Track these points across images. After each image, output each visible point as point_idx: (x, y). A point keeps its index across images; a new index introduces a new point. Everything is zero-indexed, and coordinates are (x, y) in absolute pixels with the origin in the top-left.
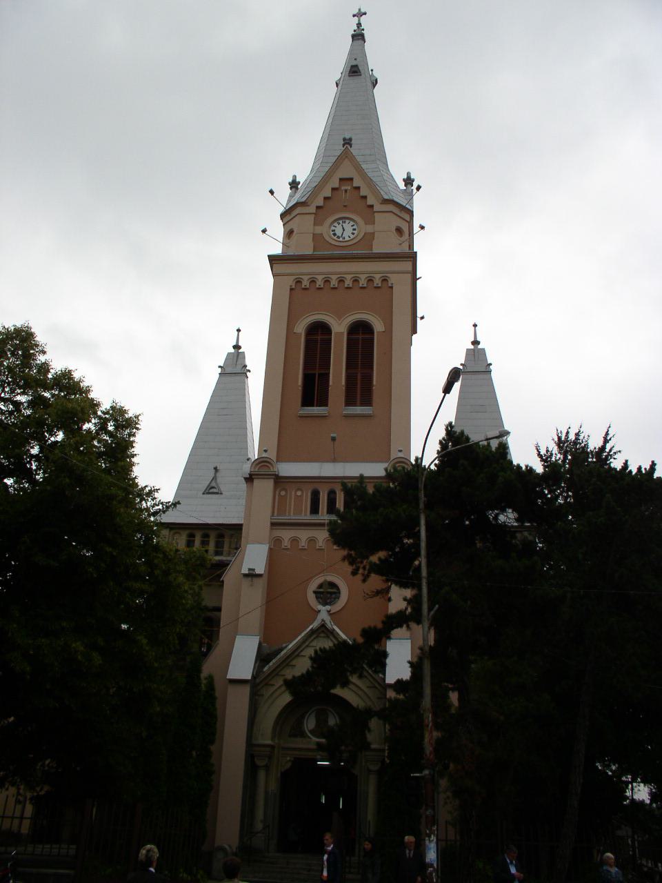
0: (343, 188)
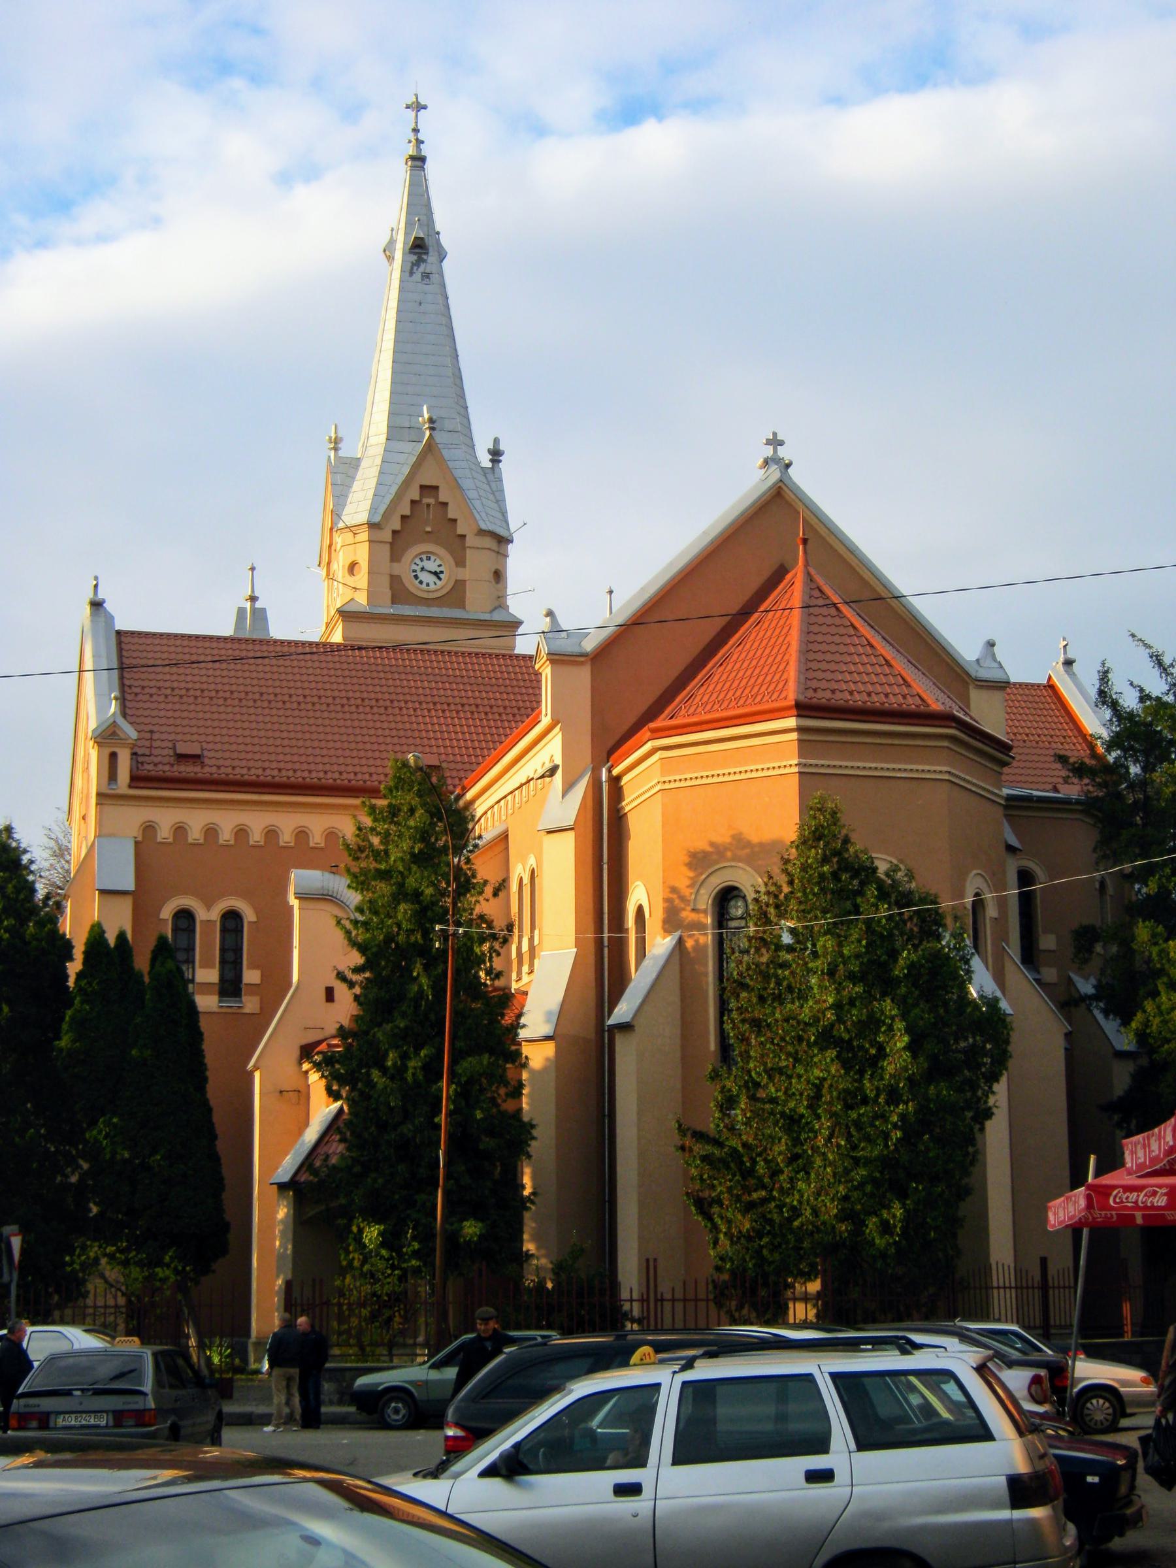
0: (426, 500)
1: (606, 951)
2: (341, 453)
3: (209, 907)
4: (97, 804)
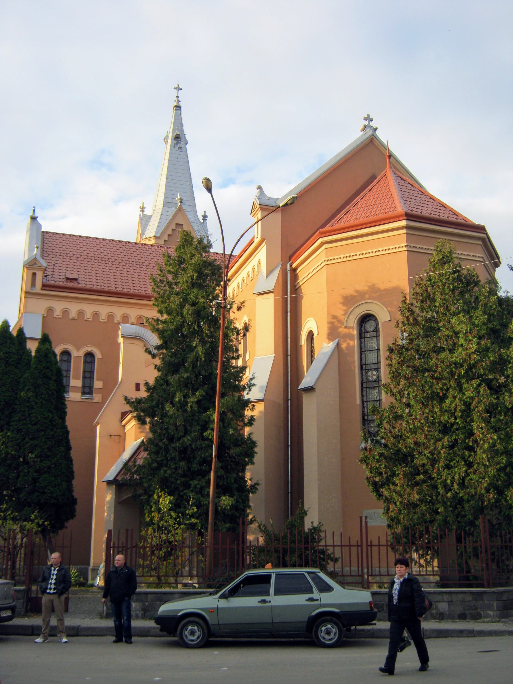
1: (289, 357)
2: (145, 213)
3: (78, 349)
4: (25, 297)
